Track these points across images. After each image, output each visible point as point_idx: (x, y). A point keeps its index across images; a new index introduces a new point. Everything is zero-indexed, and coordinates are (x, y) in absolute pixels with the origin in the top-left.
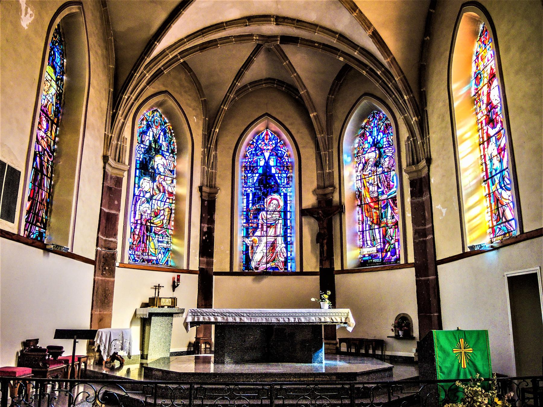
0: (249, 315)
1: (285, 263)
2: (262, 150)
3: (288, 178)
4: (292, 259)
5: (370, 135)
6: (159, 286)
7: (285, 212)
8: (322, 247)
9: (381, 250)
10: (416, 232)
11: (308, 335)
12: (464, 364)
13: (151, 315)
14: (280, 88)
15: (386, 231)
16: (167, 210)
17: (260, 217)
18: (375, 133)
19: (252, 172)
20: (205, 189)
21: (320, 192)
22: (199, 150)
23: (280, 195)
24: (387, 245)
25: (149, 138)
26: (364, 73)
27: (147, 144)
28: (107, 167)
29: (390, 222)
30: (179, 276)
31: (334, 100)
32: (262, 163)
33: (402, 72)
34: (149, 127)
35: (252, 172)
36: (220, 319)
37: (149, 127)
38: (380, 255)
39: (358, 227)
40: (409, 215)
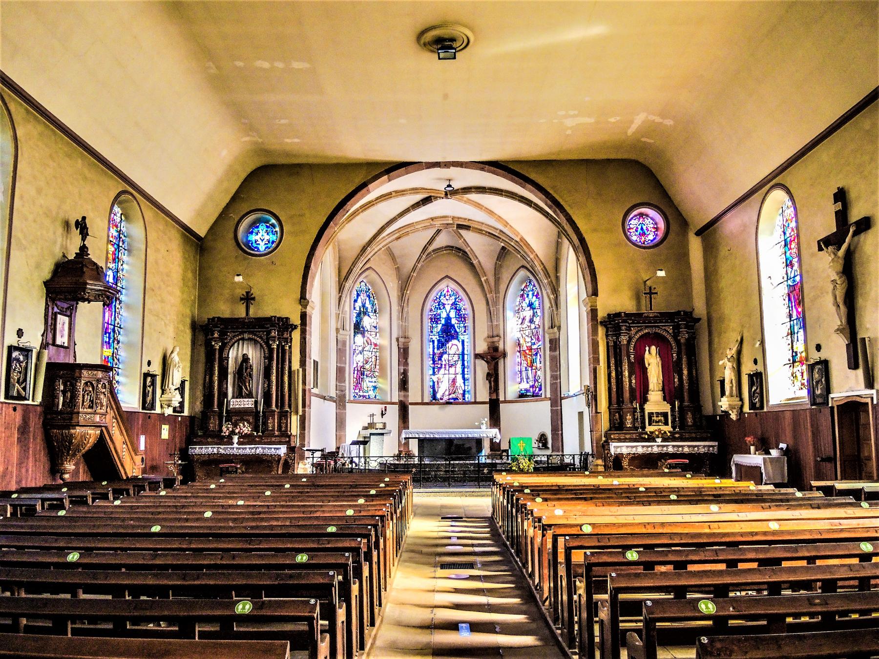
0: (438, 433)
1: (464, 395)
2: (444, 304)
3: (465, 327)
4: (468, 392)
5: (527, 297)
6: (373, 415)
7: (463, 354)
8: (490, 383)
9: (533, 386)
10: (552, 376)
11: (474, 445)
12: (522, 450)
13: (371, 434)
14: (458, 254)
15: (536, 372)
16: (374, 357)
17: (443, 359)
18: (530, 296)
19: (437, 323)
20: (400, 339)
21: (491, 340)
22: (395, 308)
23: (459, 341)
24: (537, 383)
25: (359, 304)
26: (519, 257)
27: (358, 309)
28: (339, 335)
29: (538, 365)
30: (386, 407)
31: (501, 266)
32: (444, 315)
33: (543, 264)
34: (358, 295)
35: (437, 323)
36: (421, 436)
37: (358, 295)
38: (531, 389)
39: (518, 368)
40: (548, 363)
